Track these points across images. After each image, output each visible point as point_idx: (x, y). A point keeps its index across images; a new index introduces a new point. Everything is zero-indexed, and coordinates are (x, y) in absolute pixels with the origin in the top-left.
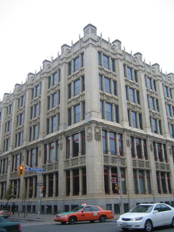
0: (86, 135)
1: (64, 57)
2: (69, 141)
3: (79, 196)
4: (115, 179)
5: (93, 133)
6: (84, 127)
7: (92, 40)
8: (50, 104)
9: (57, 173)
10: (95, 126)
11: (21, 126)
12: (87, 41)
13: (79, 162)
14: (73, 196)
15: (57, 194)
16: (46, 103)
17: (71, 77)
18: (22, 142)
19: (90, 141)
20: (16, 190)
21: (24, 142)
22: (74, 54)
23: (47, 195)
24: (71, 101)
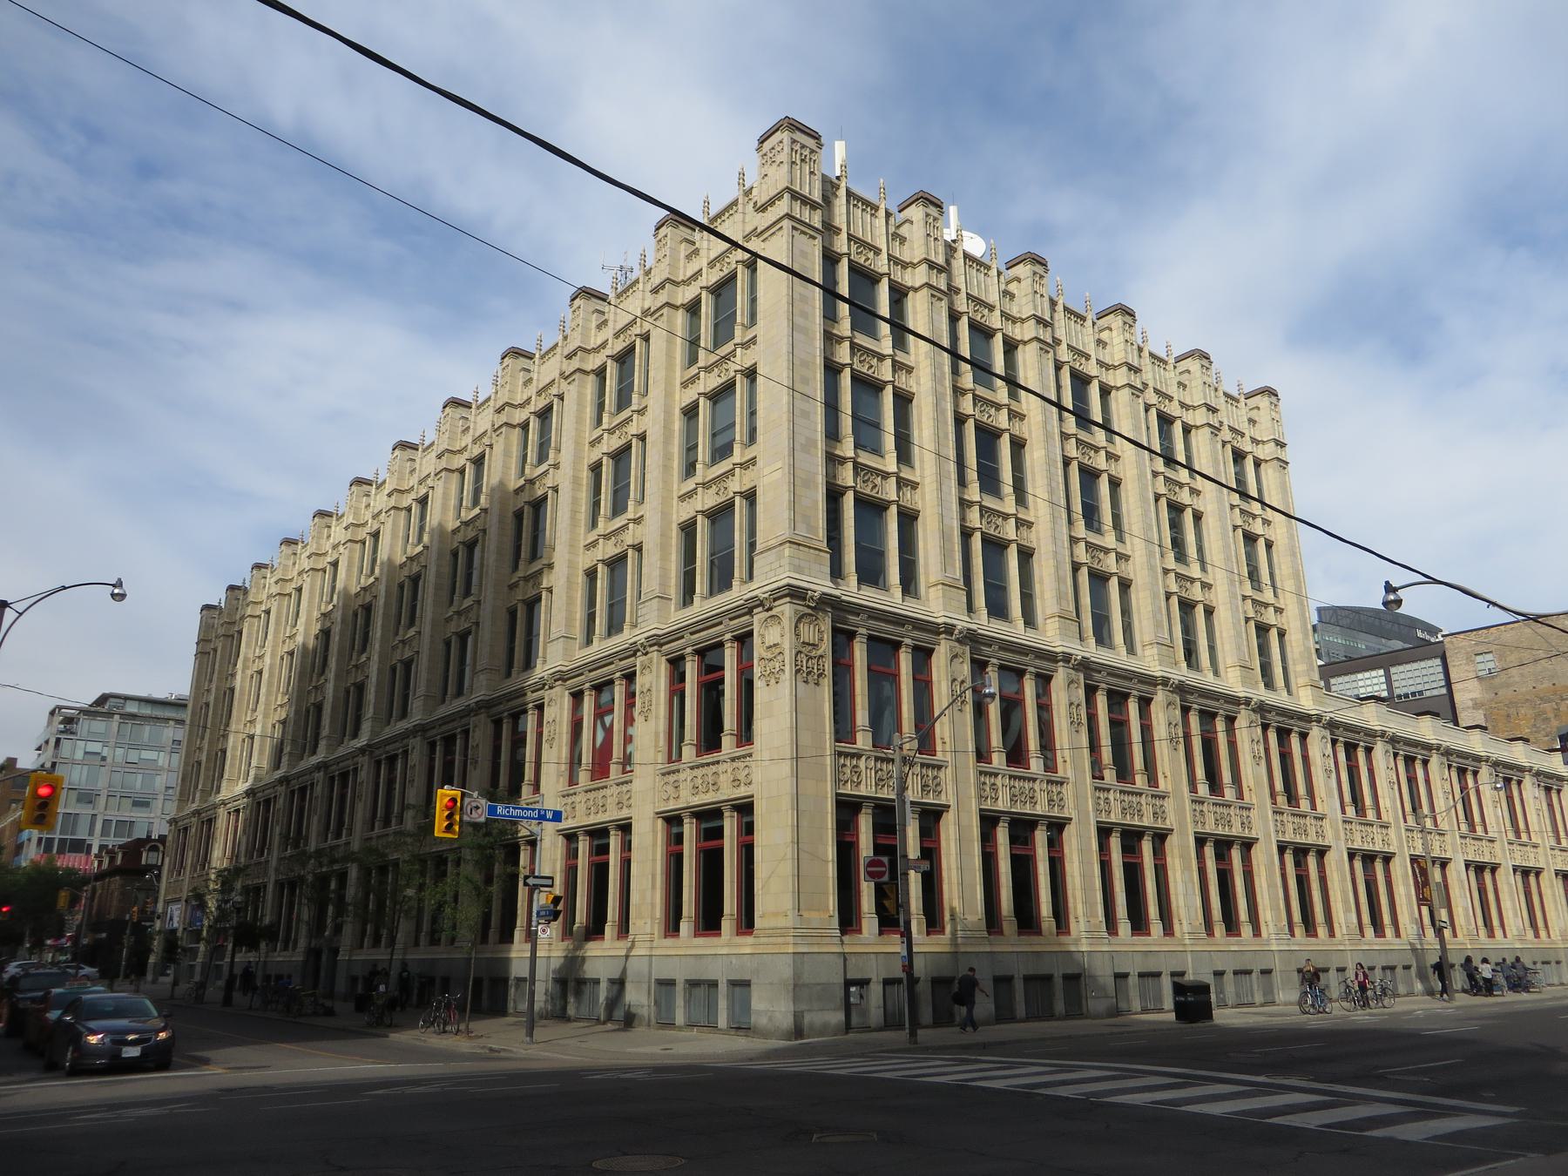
1: (668, 279)
3: (723, 937)
4: (883, 865)
5: (787, 645)
6: (633, 658)
7: (795, 196)
8: (520, 545)
9: (625, 828)
10: (796, 612)
11: (468, 602)
12: (771, 202)
13: (725, 780)
15: (747, 922)
16: (584, 495)
17: (697, 376)
21: (482, 679)
22: (712, 264)
23: (685, 927)
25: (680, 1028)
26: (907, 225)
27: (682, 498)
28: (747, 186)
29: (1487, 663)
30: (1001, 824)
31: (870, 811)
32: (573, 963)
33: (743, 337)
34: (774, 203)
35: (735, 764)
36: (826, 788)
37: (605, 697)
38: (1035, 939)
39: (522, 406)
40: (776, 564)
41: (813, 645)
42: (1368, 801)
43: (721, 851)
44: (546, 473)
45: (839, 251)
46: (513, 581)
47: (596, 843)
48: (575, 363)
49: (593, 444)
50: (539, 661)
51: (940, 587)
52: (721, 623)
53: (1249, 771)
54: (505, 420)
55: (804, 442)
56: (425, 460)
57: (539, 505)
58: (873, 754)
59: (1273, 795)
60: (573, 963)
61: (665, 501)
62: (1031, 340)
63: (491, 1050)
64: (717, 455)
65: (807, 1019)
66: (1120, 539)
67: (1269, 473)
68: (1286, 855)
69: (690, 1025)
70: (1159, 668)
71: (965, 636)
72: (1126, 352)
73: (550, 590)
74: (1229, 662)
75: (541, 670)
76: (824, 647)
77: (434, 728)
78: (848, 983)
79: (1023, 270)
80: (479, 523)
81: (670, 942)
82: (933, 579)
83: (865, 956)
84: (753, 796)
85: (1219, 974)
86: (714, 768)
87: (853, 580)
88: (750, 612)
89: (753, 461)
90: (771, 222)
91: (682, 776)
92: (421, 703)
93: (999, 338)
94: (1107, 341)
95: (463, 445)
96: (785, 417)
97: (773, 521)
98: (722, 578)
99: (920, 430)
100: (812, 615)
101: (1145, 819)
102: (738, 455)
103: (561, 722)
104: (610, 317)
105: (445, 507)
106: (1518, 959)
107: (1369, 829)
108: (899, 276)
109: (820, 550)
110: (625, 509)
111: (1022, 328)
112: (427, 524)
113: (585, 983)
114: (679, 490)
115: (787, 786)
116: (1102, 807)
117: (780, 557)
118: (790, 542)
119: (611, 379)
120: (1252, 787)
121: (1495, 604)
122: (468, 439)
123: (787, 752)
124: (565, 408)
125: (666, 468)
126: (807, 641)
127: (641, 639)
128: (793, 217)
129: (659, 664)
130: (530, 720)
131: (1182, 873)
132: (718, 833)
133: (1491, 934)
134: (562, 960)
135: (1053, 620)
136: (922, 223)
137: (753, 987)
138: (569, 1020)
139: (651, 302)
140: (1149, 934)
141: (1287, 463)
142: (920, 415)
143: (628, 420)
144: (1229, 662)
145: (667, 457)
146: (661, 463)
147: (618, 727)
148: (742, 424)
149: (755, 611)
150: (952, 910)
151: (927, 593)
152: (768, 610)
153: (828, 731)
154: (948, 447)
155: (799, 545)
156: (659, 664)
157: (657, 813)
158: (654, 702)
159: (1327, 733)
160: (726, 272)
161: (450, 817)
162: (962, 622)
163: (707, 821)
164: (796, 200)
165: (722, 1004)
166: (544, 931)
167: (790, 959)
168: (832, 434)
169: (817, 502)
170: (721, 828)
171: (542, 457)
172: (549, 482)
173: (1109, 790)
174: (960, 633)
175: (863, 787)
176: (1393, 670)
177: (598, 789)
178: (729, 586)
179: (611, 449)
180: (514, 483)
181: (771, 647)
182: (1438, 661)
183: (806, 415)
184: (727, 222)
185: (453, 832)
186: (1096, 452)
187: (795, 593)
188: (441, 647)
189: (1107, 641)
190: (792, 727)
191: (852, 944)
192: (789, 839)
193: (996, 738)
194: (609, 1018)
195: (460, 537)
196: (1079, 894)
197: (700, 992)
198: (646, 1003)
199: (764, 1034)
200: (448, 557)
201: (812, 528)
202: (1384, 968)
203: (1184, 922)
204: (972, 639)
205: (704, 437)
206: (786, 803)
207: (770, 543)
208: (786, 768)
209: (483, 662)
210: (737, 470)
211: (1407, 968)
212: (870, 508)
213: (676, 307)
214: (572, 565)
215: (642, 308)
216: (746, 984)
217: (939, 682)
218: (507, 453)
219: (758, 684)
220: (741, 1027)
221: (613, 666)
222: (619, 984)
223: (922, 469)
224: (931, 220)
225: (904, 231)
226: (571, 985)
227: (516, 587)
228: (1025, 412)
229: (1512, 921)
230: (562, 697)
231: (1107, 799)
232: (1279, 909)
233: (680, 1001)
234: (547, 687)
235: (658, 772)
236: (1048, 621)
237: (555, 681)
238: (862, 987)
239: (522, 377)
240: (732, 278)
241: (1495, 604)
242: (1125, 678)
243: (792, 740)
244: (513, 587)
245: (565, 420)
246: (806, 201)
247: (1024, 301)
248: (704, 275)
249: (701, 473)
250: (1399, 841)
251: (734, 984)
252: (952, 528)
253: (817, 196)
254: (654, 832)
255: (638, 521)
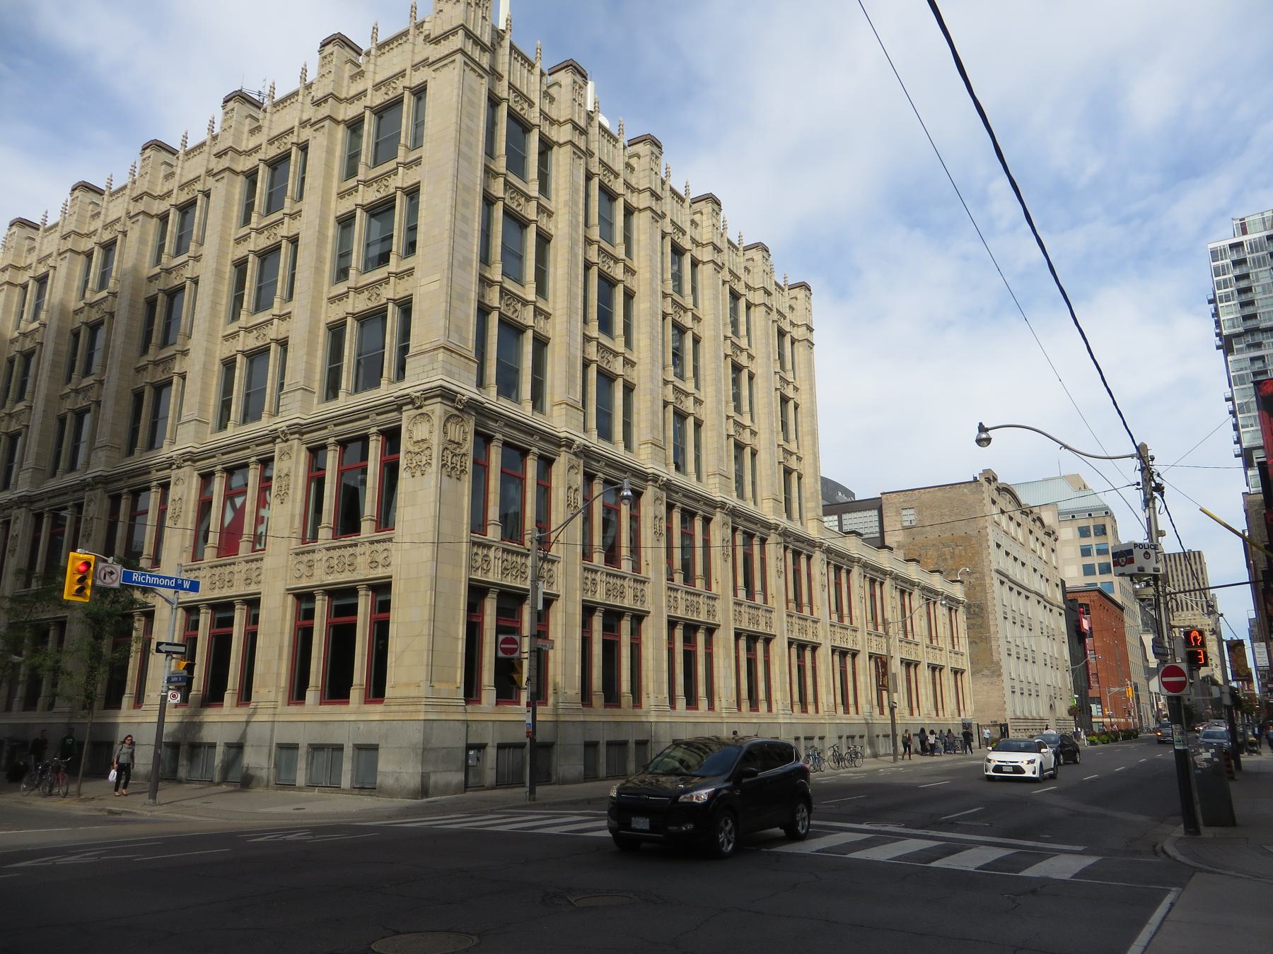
0: (402, 448)
1: (146, 192)
2: (65, 521)
3: (351, 705)
5: (436, 441)
6: (80, 494)
7: (469, 35)
9: (253, 603)
10: (446, 412)
11: (89, 381)
12: (445, 36)
13: (238, 579)
14: (289, 704)
15: (377, 690)
16: (226, 289)
18: (89, 456)
19: (418, 473)
20: (1188, 617)
21: (101, 455)
23: (311, 695)
24: (346, 295)
25: (300, 789)
26: (556, 87)
27: (332, 300)
28: (419, 20)
29: (909, 516)
30: (597, 614)
31: (495, 596)
32: (191, 726)
33: (406, 157)
34: (447, 37)
35: (248, 566)
36: (461, 573)
37: (237, 481)
38: (616, 711)
39: (162, 198)
40: (430, 367)
41: (458, 443)
42: (846, 611)
43: (230, 637)
44: (185, 264)
45: (500, 95)
46: (141, 364)
47: (218, 616)
48: (225, 162)
49: (238, 241)
50: (166, 442)
51: (564, 406)
52: (367, 417)
53: (773, 583)
54: (142, 209)
55: (461, 260)
56: (46, 240)
57: (174, 294)
58: (500, 545)
59: (787, 602)
60: (191, 726)
61: (315, 301)
62: (645, 209)
63: (111, 812)
64: (370, 265)
65: (433, 779)
66: (697, 387)
67: (800, 349)
68: (792, 649)
69: (311, 786)
70: (719, 494)
71: (581, 451)
72: (713, 235)
73: (183, 376)
74: (765, 495)
75: (167, 451)
76: (467, 446)
77: (42, 500)
78: (469, 747)
79: (643, 149)
80: (38, 337)
81: (294, 709)
82: (557, 399)
83: (484, 723)
84: (391, 577)
85: (797, 739)
86: (351, 550)
87: (493, 391)
88: (399, 409)
89: (410, 272)
90: (443, 55)
91: (317, 556)
92: (28, 475)
93: (532, 229)
94: (698, 222)
95: (92, 229)
96: (446, 234)
97: (425, 331)
98: (369, 375)
99: (556, 268)
100: (459, 417)
101: (701, 615)
102: (394, 265)
103: (188, 500)
104: (266, 124)
105: (67, 287)
106: (949, 731)
107: (845, 631)
108: (546, 128)
109: (469, 359)
110: (270, 305)
111: (638, 198)
112: (46, 302)
113: (200, 747)
114: (330, 292)
115: (428, 569)
116: (671, 604)
117: (432, 361)
118: (444, 348)
119: (262, 182)
120: (774, 595)
121: (1066, 447)
122: (98, 224)
123: (430, 537)
124: (211, 204)
125: (318, 270)
126: (453, 439)
127: (283, 426)
128: (466, 53)
129: (299, 451)
130: (153, 498)
131: (724, 659)
132: (229, 622)
133: (847, 711)
134: (176, 726)
135: (646, 446)
136: (570, 88)
137: (381, 751)
138: (180, 782)
139: (310, 113)
140: (697, 709)
141: (813, 345)
142: (556, 256)
143: (280, 222)
144: (765, 495)
145: (320, 260)
146: (313, 265)
147: (250, 507)
148: (399, 237)
149: (404, 408)
150: (555, 685)
151: (552, 410)
152: (418, 408)
153: (465, 521)
154: (577, 286)
155: (452, 351)
156: (299, 451)
157: (288, 590)
158: (291, 486)
159: (824, 557)
160: (391, 95)
161: (82, 580)
162: (580, 439)
163: (337, 599)
164: (469, 39)
165: (347, 766)
166: (174, 696)
167: (420, 726)
168: (485, 260)
169: (469, 315)
170: (355, 606)
171: (180, 249)
172: (188, 272)
173: (677, 590)
174: (578, 447)
175: (490, 574)
176: (844, 516)
177: (225, 565)
178: (378, 385)
179: (258, 249)
180: (148, 269)
181: (418, 442)
182: (875, 512)
183: (464, 235)
184: (395, 50)
185: (84, 596)
186: (685, 312)
187: (447, 395)
188: (54, 423)
189: (682, 469)
190: (435, 516)
191: (474, 713)
192: (426, 617)
193: (597, 540)
194: (224, 780)
195: (82, 318)
196: (651, 674)
197: (323, 757)
198: (265, 765)
199: (391, 793)
200: (68, 336)
201: (464, 339)
202: (848, 737)
203: (723, 699)
204: (585, 453)
205: (359, 245)
206: (425, 585)
207: (424, 347)
208: (427, 552)
209: (102, 439)
210: (392, 279)
211: (862, 737)
212: (511, 329)
213: (338, 122)
214: (209, 353)
215: (300, 119)
216: (374, 748)
217: (557, 488)
218: (142, 241)
219: (403, 475)
220: (366, 785)
221: (215, 459)
222: (237, 748)
223: (555, 302)
224: (577, 87)
225: (553, 91)
226: (183, 750)
227: (144, 370)
228: (636, 269)
229: (924, 704)
230: (191, 476)
231: (676, 597)
232: (786, 691)
233: (302, 764)
234: (174, 467)
235: (291, 552)
236: (642, 447)
237: (184, 461)
238: (479, 751)
239: (163, 170)
240: (398, 102)
241: (1066, 447)
242: (694, 499)
243: (434, 528)
244: (139, 370)
245: (210, 216)
246: (477, 42)
247: (642, 174)
248: (369, 96)
249: (244, 319)
250: (863, 643)
251: (359, 748)
252: (576, 357)
253: (487, 39)
254: (284, 607)
255: (284, 317)
